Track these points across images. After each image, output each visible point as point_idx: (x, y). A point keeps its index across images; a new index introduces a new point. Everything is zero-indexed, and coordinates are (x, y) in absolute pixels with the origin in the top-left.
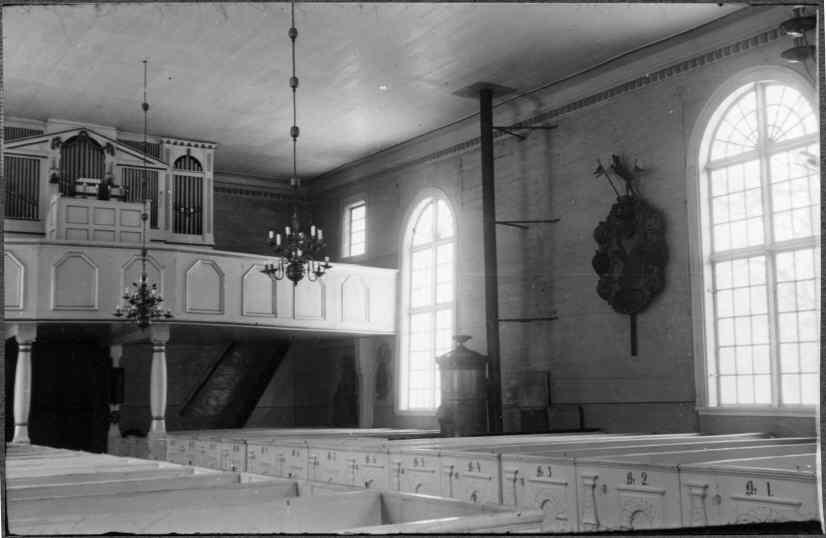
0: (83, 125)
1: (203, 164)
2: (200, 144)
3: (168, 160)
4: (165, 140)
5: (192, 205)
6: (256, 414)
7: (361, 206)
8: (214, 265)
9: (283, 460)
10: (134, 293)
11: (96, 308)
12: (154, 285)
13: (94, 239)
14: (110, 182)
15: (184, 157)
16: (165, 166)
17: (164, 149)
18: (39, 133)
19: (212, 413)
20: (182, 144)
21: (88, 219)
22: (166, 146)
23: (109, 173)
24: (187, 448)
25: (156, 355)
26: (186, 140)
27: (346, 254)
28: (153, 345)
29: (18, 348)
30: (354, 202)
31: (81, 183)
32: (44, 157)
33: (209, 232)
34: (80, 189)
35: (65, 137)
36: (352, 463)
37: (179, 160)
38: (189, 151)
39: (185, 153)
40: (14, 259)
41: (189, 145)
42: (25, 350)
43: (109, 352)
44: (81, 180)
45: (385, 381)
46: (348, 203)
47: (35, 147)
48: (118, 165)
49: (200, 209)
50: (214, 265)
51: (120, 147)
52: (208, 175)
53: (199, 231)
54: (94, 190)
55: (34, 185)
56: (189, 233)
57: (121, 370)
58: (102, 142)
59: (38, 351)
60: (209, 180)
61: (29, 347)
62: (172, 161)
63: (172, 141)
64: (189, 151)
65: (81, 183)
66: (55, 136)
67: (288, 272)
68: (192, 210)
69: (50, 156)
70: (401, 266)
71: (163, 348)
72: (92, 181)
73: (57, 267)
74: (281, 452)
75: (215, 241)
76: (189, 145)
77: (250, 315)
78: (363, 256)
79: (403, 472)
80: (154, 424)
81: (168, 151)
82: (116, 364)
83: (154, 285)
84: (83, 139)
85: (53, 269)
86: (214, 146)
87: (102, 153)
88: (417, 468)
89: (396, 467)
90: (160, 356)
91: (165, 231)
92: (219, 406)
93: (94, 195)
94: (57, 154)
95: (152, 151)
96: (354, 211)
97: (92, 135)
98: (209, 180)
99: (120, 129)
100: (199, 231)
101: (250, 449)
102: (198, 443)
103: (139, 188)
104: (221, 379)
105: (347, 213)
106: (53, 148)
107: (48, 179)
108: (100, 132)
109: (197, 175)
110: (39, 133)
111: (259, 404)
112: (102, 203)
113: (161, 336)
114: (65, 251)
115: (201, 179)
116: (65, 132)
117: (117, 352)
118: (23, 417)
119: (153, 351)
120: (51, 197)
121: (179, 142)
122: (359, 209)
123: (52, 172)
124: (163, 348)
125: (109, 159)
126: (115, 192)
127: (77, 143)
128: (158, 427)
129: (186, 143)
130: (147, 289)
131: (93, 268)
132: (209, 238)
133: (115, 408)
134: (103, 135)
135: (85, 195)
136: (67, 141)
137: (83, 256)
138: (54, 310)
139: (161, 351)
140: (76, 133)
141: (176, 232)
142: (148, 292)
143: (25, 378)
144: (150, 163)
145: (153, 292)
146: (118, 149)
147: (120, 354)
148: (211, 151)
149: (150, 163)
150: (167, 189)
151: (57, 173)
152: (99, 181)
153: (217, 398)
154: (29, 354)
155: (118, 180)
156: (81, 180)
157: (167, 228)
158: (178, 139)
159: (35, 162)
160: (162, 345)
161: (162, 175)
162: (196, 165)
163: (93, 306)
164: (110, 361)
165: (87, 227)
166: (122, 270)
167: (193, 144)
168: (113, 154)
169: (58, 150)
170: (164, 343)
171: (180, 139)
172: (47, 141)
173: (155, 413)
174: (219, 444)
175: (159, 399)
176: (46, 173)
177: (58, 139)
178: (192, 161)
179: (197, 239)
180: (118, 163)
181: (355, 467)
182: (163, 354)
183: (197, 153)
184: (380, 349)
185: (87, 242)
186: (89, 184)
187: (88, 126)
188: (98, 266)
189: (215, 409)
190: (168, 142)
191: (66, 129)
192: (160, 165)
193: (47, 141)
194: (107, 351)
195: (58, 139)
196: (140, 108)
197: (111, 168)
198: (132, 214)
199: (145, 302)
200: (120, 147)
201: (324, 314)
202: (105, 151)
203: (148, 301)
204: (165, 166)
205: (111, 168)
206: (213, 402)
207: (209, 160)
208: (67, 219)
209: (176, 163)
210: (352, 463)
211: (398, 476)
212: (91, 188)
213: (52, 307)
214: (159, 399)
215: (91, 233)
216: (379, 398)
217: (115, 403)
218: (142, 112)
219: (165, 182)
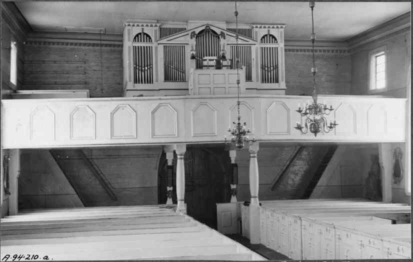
0: (205, 22)
1: (277, 38)
2: (275, 26)
3: (256, 38)
4: (254, 26)
5: (272, 65)
9: (321, 233)
10: (234, 128)
14: (224, 58)
15: (266, 35)
17: (254, 31)
19: (289, 188)
20: (265, 27)
22: (255, 30)
23: (223, 50)
24: (270, 216)
26: (267, 24)
28: (250, 153)
29: (258, 155)
31: (206, 60)
34: (205, 63)
35: (197, 31)
36: (360, 243)
37: (264, 37)
38: (269, 30)
39: (266, 33)
40: (171, 107)
41: (269, 27)
42: (181, 159)
44: (205, 58)
48: (228, 44)
49: (276, 67)
52: (281, 45)
53: (277, 81)
54: (213, 63)
55: (182, 61)
57: (236, 165)
58: (218, 31)
60: (281, 48)
61: (183, 157)
63: (259, 26)
64: (269, 30)
65: (206, 60)
66: (192, 31)
67: (311, 128)
68: (272, 68)
69: (190, 44)
71: (256, 155)
75: (287, 86)
76: (269, 27)
77: (271, 133)
79: (391, 254)
80: (252, 199)
81: (256, 32)
82: (233, 162)
84: (207, 32)
85: (192, 113)
86: (284, 26)
88: (399, 253)
89: (387, 250)
91: (256, 83)
92: (294, 184)
93: (212, 66)
95: (248, 33)
97: (212, 28)
98: (281, 48)
99: (227, 22)
100: (277, 81)
101: (304, 223)
102: (275, 215)
103: (240, 60)
104: (296, 168)
106: (192, 38)
107: (190, 57)
108: (216, 25)
109: (274, 46)
111: (319, 184)
112: (218, 71)
113: (254, 148)
116: (197, 28)
117: (233, 154)
118: (182, 196)
119: (250, 157)
121: (263, 26)
123: (192, 53)
125: (222, 41)
126: (225, 63)
127: (204, 33)
129: (267, 26)
130: (241, 125)
131: (213, 110)
133: (233, 187)
136: (198, 34)
137: (208, 104)
139: (254, 157)
140: (204, 28)
141: (263, 82)
142: (242, 127)
144: (246, 41)
146: (227, 34)
147: (235, 156)
148: (282, 30)
149: (246, 41)
150: (257, 57)
151: (194, 53)
152: (215, 58)
153: (293, 180)
154: (183, 160)
155: (228, 56)
156: (205, 58)
157: (258, 81)
158: (263, 24)
159: (182, 47)
160: (254, 153)
161: (253, 48)
162: (274, 39)
163: (214, 133)
165: (209, 86)
166: (230, 111)
167: (271, 26)
169: (194, 39)
172: (188, 34)
173: (252, 194)
175: (255, 188)
178: (271, 37)
180: (227, 44)
181: (362, 245)
182: (256, 159)
183: (273, 32)
187: (210, 22)
189: (292, 187)
190: (257, 27)
192: (251, 42)
193: (188, 34)
194: (228, 153)
195: (194, 32)
196: (234, 15)
197: (224, 46)
198: (231, 77)
201: (355, 132)
202: (220, 37)
203: (242, 133)
205: (224, 46)
206: (290, 182)
207: (281, 37)
208: (198, 82)
210: (360, 243)
212: (212, 62)
213: (192, 135)
214: (255, 188)
216: (395, 183)
217: (233, 184)
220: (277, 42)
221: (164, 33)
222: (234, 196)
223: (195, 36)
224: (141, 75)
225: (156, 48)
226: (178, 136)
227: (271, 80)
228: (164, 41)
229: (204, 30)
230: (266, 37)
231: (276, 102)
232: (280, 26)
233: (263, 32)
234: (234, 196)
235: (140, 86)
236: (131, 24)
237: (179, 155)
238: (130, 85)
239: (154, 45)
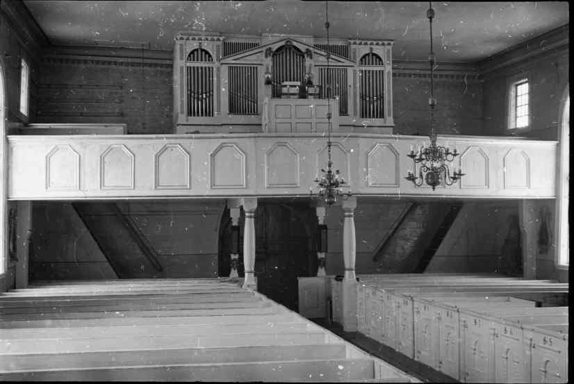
1: (382, 58)
2: (380, 43)
3: (355, 58)
4: (352, 42)
6: (434, 261)
7: (526, 82)
8: (391, 147)
10: (323, 177)
11: (298, 185)
12: (338, 171)
13: (296, 131)
14: (310, 83)
15: (368, 55)
16: (352, 64)
18: (255, 45)
20: (366, 44)
21: (291, 115)
25: (347, 219)
27: (512, 126)
28: (344, 212)
29: (354, 213)
30: (518, 80)
31: (285, 86)
32: (261, 65)
33: (389, 115)
35: (275, 47)
37: (364, 57)
38: (371, 49)
41: (372, 44)
42: (250, 217)
43: (315, 212)
44: (285, 83)
45: (546, 238)
46: (514, 81)
47: (254, 57)
48: (316, 66)
49: (381, 98)
50: (391, 147)
51: (316, 51)
52: (388, 68)
53: (382, 115)
56: (374, 117)
57: (325, 227)
58: (303, 48)
59: (259, 218)
61: (253, 214)
62: (358, 59)
64: (371, 49)
66: (267, 47)
67: (427, 179)
70: (560, 136)
71: (352, 214)
72: (292, 83)
73: (269, 155)
74: (438, 312)
75: (395, 123)
78: (526, 128)
80: (347, 273)
82: (321, 222)
83: (338, 171)
85: (265, 156)
86: (392, 43)
87: (304, 57)
90: (350, 221)
94: (269, 62)
96: (519, 87)
99: (315, 37)
100: (382, 115)
103: (330, 87)
105: (513, 89)
106: (266, 57)
110: (255, 45)
111: (436, 254)
114: (275, 141)
115: (383, 71)
117: (321, 213)
119: (345, 216)
120: (264, 92)
121: (363, 42)
122: (524, 85)
124: (346, 214)
125: (308, 62)
126: (311, 90)
127: (284, 50)
128: (350, 277)
129: (369, 42)
132: (390, 121)
133: (321, 255)
134: (303, 42)
135: (289, 95)
138: (267, 187)
139: (350, 216)
140: (283, 43)
141: (363, 117)
143: (251, 238)
144: (340, 61)
145: (337, 176)
146: (315, 53)
149: (340, 61)
152: (299, 83)
154: (253, 219)
157: (355, 114)
159: (253, 70)
161: (350, 72)
163: (296, 184)
164: (316, 218)
165: (310, 121)
167: (375, 43)
168: (311, 58)
169: (270, 58)
170: (352, 209)
171: (363, 40)
173: (347, 266)
174: (392, 296)
176: (262, 76)
177: (270, 48)
178: (203, 53)
179: (378, 122)
180: (314, 66)
183: (379, 50)
184: (541, 212)
185: (290, 134)
186: (291, 86)
187: (292, 36)
188: (299, 153)
190: (355, 43)
191: (274, 40)
192: (347, 63)
195: (270, 49)
197: (310, 68)
199: (331, 184)
200: (316, 51)
201: (487, 184)
202: (306, 56)
203: (333, 184)
204: (352, 64)
206: (399, 250)
209: (361, 60)
211: (530, 351)
212: (294, 88)
213: (266, 186)
215: (294, 126)
217: (321, 252)
218: (324, 29)
219: (354, 76)
220: (382, 64)
221: (229, 49)
222: (235, 269)
223: (272, 54)
224: (197, 105)
225: (218, 69)
226: (190, 188)
227: (202, 112)
228: (230, 60)
229: (284, 46)
230: (196, 53)
231: (380, 143)
232: (386, 42)
233: (365, 50)
234: (235, 269)
235: (194, 120)
236: (185, 37)
237: (248, 212)
238: (182, 118)
239: (215, 64)
